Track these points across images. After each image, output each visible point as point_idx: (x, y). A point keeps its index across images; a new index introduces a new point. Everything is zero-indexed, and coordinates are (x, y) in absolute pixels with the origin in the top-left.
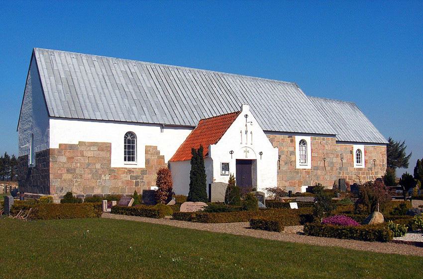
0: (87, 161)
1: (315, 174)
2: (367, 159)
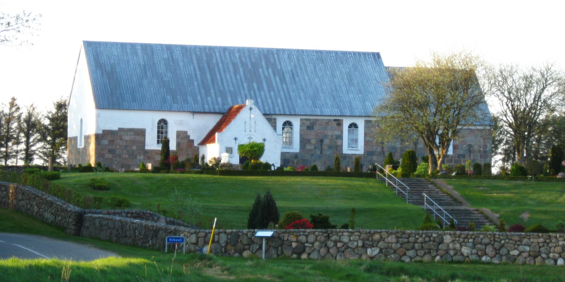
0: (125, 144)
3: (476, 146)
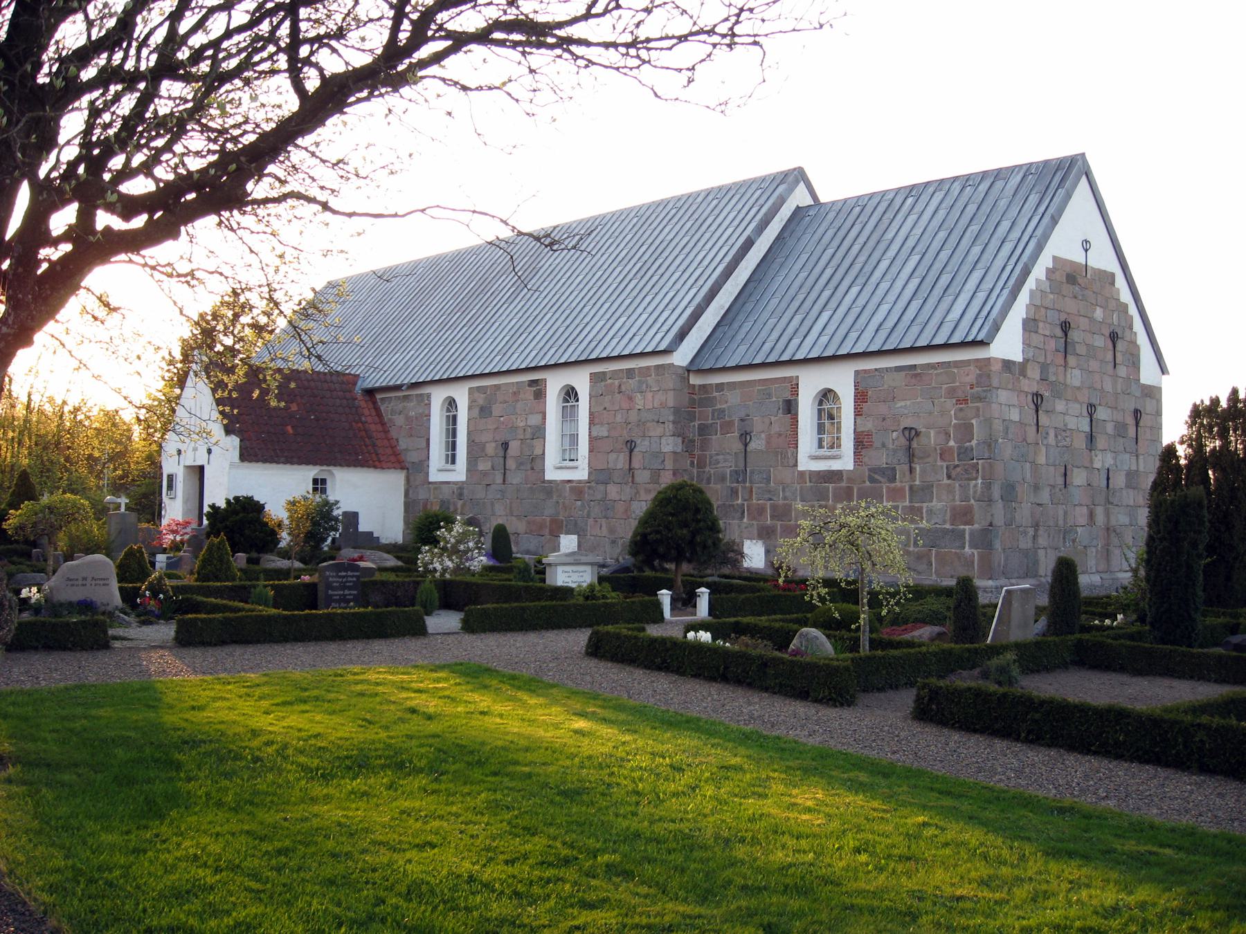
1: (599, 497)
2: (868, 425)
3: (932, 433)
